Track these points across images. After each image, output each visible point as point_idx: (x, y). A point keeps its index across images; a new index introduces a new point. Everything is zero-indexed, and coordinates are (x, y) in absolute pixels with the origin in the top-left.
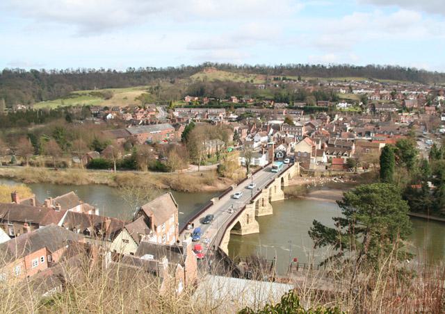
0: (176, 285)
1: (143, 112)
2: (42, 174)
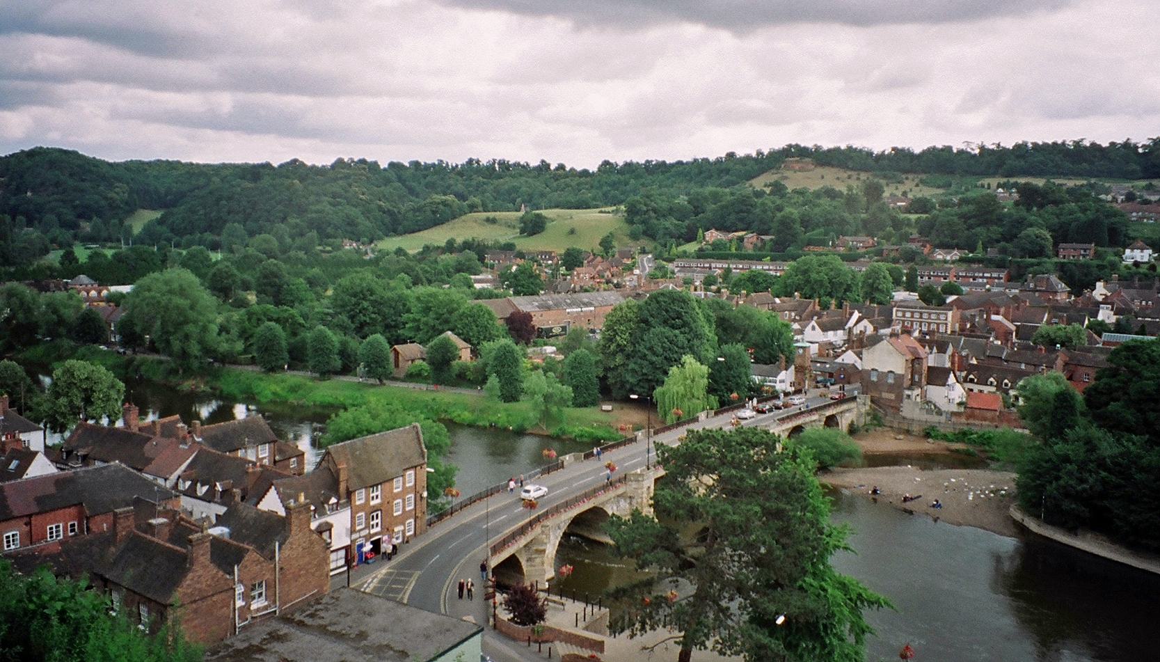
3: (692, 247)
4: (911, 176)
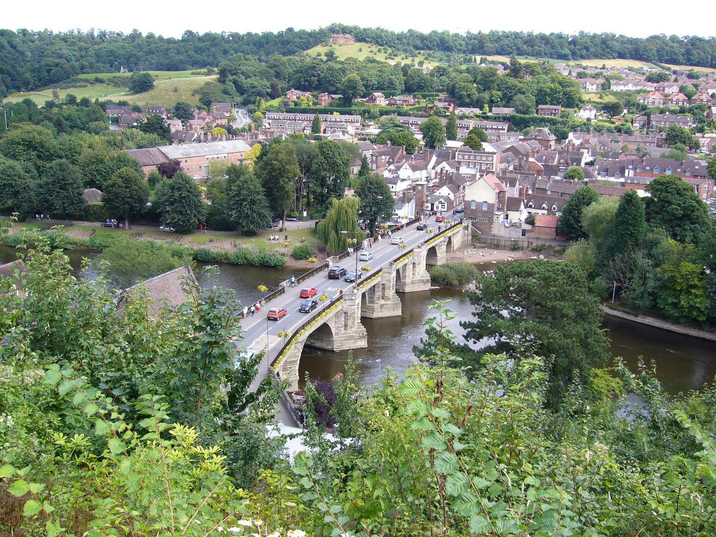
0: (122, 530)
1: (204, 119)
2: (392, 56)
3: (275, 102)
4: (422, 52)
